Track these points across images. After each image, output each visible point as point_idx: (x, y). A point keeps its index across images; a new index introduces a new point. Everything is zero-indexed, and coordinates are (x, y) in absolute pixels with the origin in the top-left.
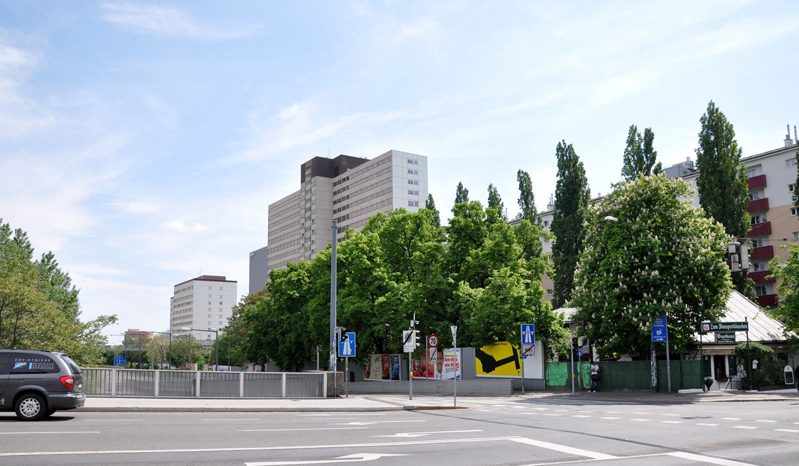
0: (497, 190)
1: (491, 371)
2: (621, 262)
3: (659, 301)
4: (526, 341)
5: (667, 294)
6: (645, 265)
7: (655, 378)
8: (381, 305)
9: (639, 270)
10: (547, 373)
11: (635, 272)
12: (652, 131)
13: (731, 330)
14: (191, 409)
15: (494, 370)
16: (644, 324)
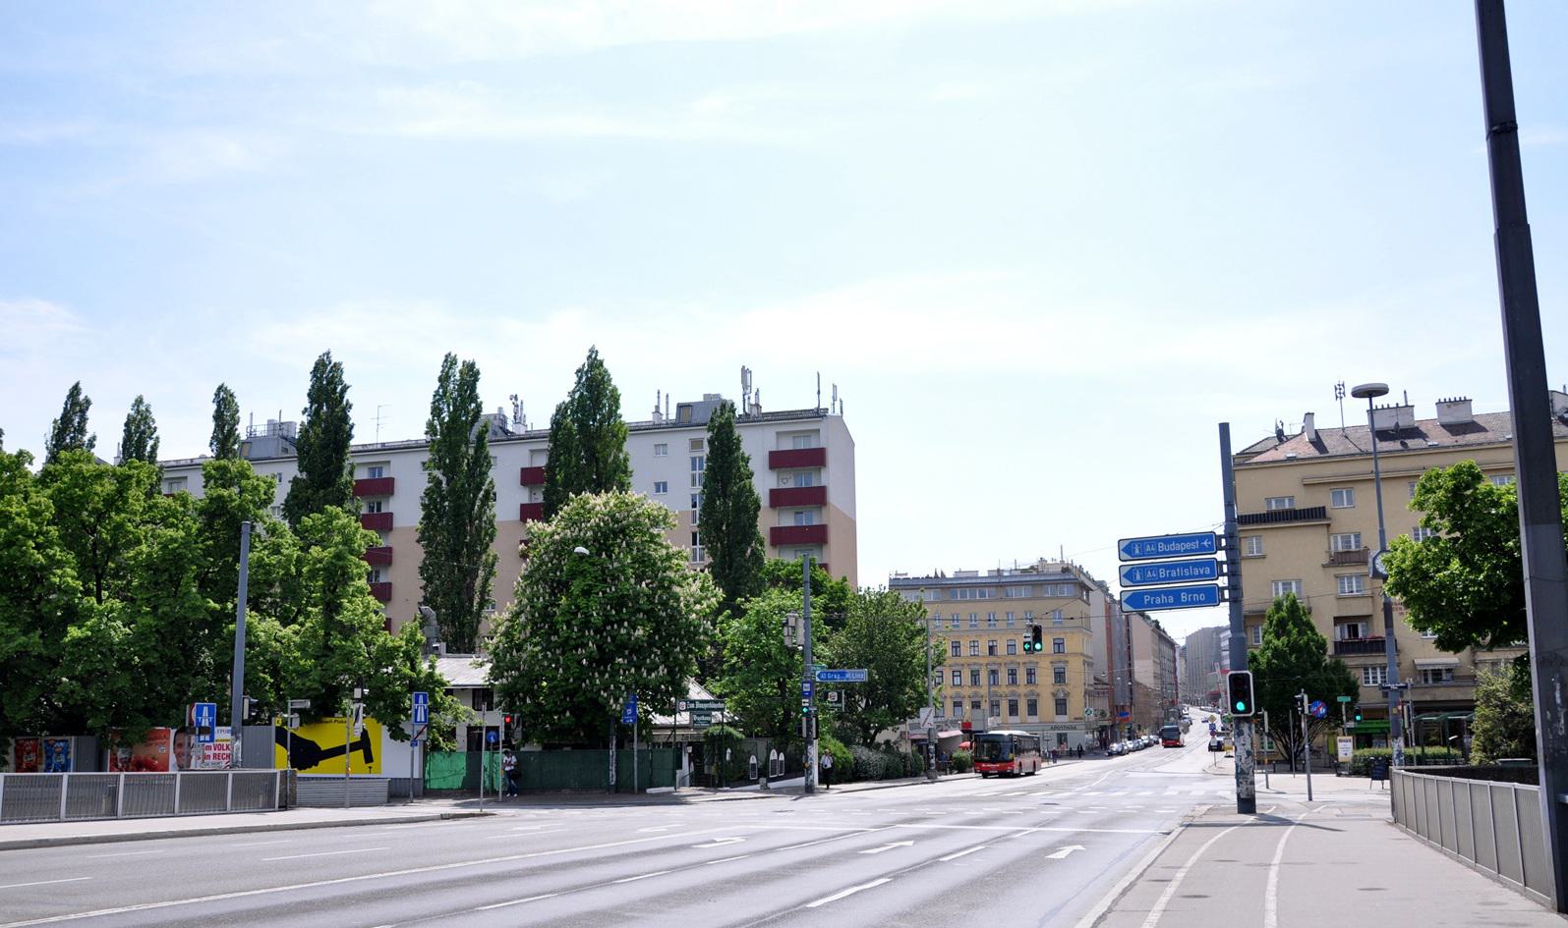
0: (151, 410)
1: (310, 767)
2: (595, 615)
3: (638, 669)
4: (418, 720)
5: (648, 661)
6: (623, 621)
7: (614, 773)
8: (78, 643)
9: (616, 626)
10: (427, 768)
11: (609, 628)
12: (477, 366)
13: (708, 709)
14: (231, 829)
15: (316, 765)
16: (616, 700)
